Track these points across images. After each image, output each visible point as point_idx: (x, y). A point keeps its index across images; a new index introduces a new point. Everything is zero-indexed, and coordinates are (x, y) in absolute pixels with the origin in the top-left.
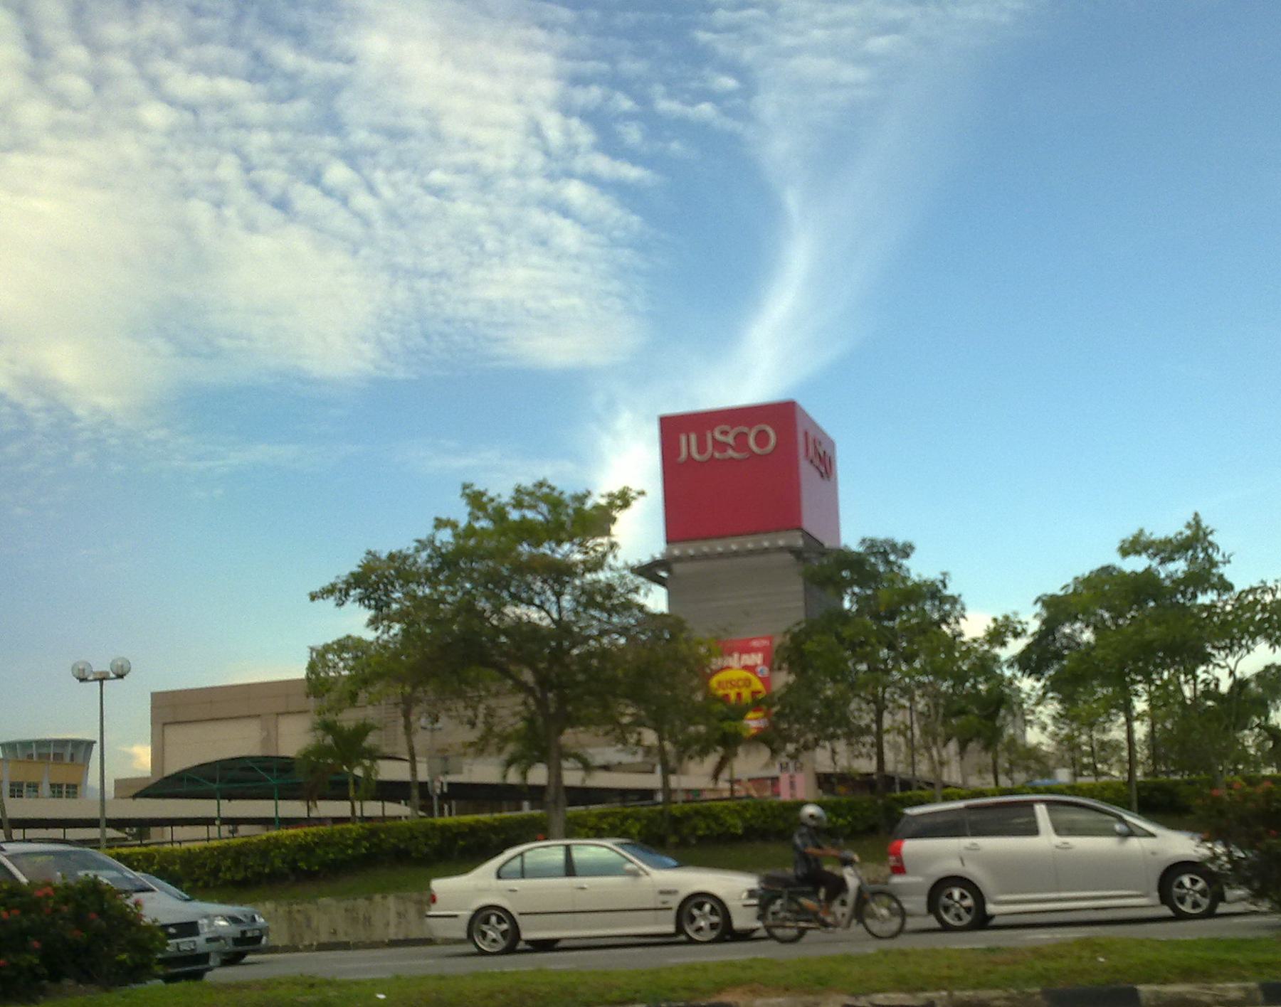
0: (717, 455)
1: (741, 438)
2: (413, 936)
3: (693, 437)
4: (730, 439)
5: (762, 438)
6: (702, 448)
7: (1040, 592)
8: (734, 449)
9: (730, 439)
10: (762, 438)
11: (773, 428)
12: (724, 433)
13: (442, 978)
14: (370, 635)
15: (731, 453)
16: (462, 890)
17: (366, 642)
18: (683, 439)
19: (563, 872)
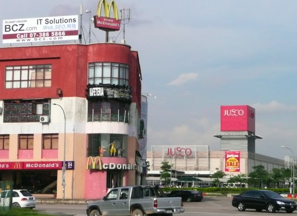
0: (232, 115)
1: (237, 113)
2: (23, 58)
3: (227, 111)
4: (235, 112)
5: (241, 112)
6: (229, 113)
7: (85, 156)
8: (235, 114)
9: (235, 112)
10: (241, 112)
11: (243, 110)
12: (234, 111)
13: (76, 105)
14: (73, 119)
15: (235, 115)
16: (204, 188)
17: (41, 88)
18: (225, 111)
19: (102, 138)
